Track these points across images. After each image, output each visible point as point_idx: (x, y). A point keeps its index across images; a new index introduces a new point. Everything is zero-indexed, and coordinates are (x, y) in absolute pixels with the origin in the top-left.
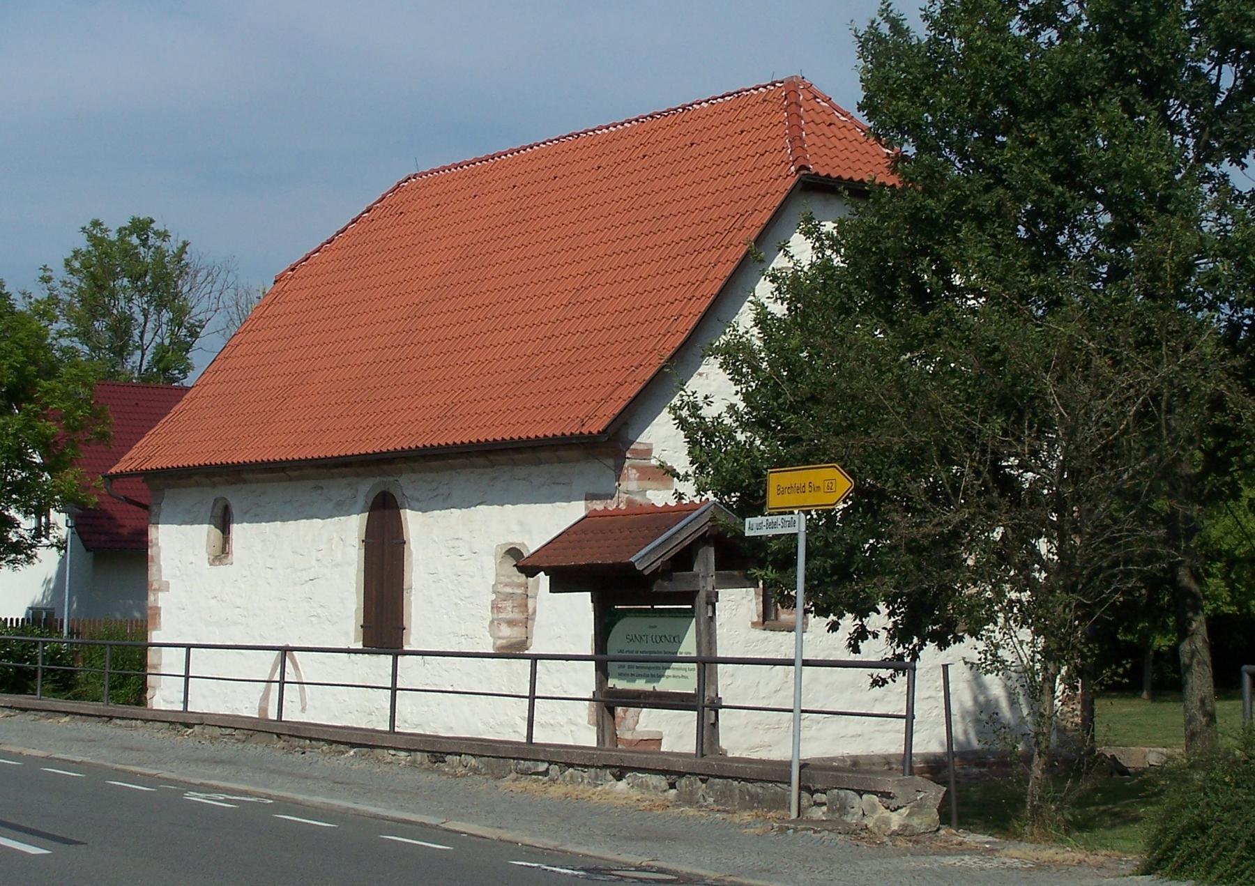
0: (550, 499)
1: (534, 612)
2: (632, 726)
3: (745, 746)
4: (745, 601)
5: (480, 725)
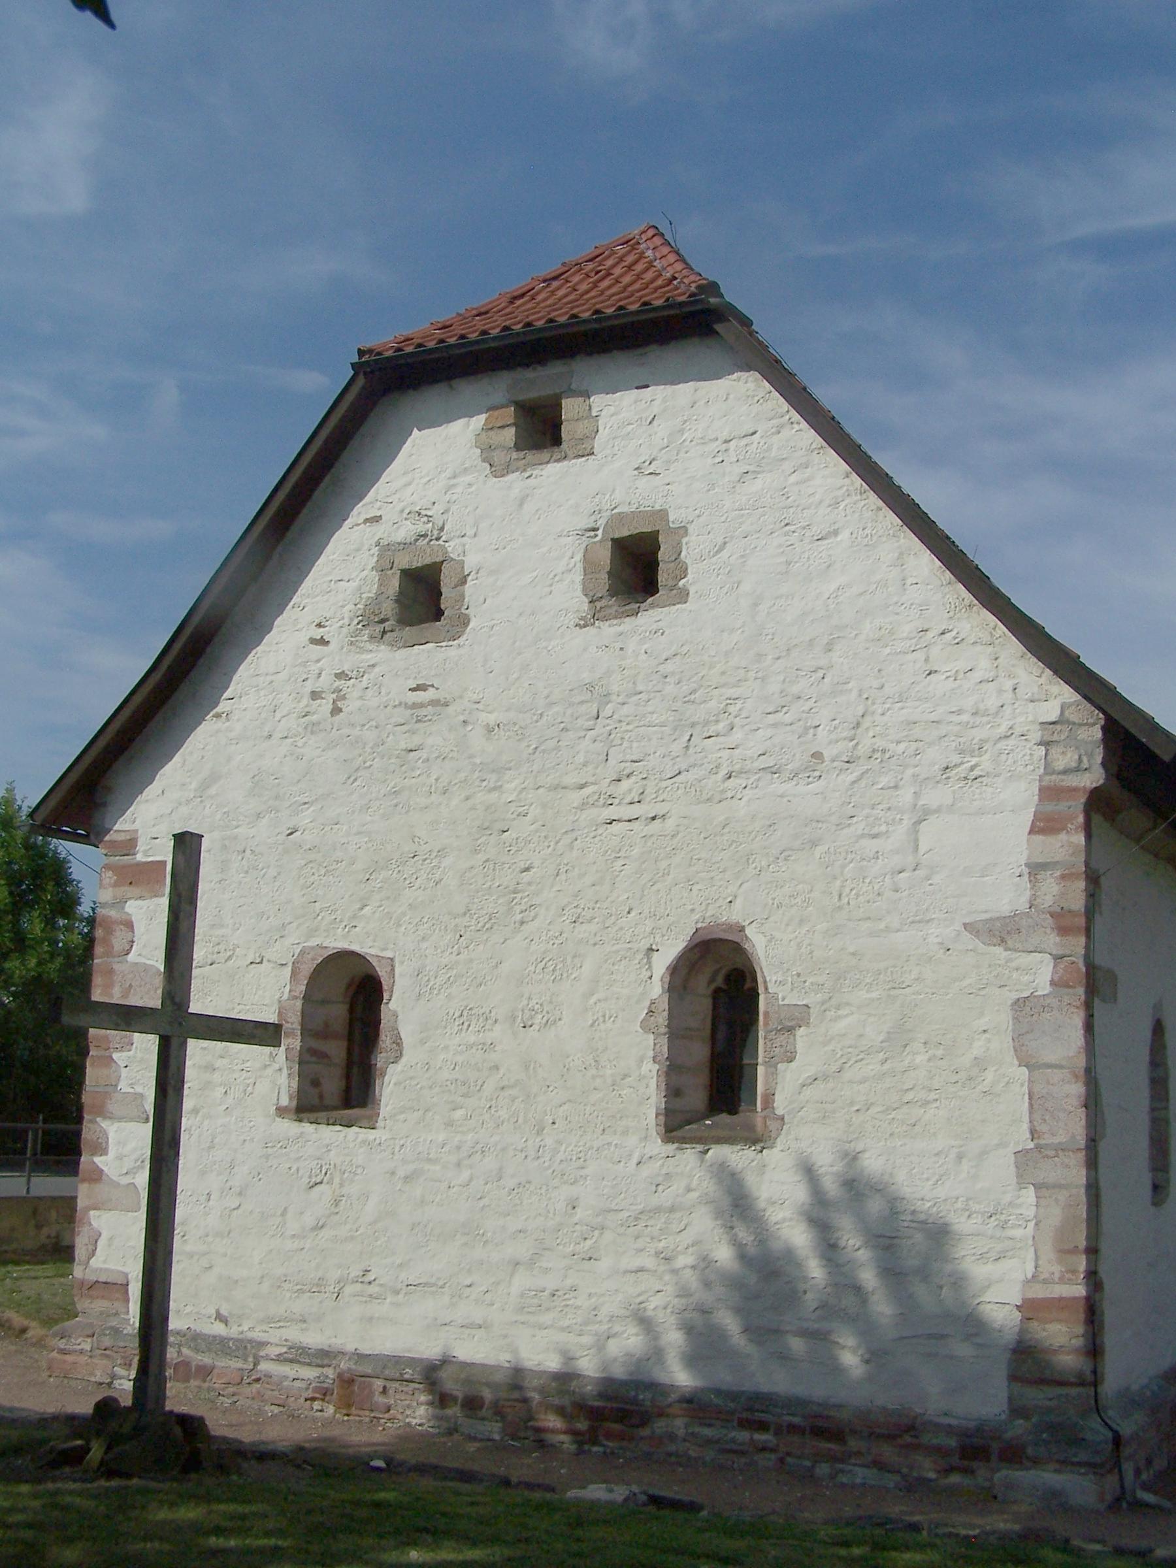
4: (269, 1071)
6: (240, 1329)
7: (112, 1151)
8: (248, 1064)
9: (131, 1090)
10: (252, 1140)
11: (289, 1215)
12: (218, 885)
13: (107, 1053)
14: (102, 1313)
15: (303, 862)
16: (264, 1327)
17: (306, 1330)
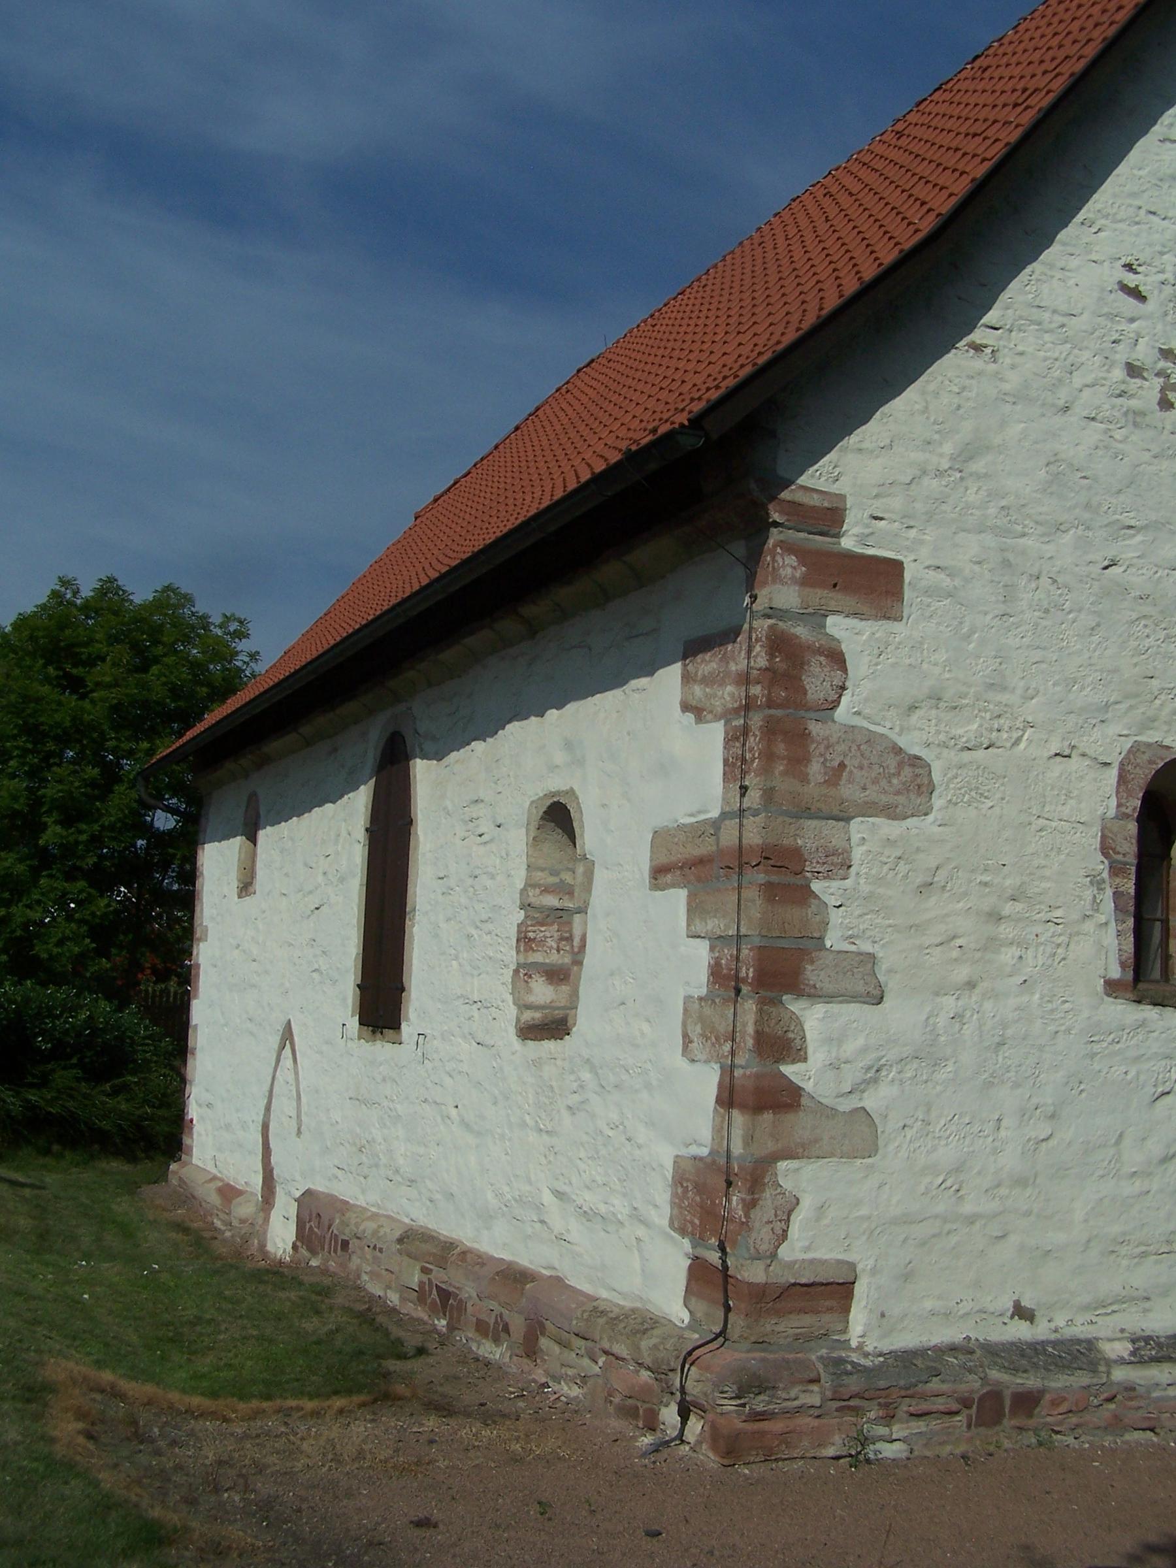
0: (617, 680)
1: (583, 946)
2: (764, 1247)
3: (1085, 1298)
4: (1089, 926)
5: (490, 1195)
6: (1052, 1325)
7: (817, 1056)
8: (1058, 913)
9: (853, 948)
10: (1068, 1031)
11: (1127, 1142)
12: (996, 622)
13: (798, 880)
14: (797, 1338)
15: (1134, 616)
16: (1089, 1316)
17: (1146, 1311)
